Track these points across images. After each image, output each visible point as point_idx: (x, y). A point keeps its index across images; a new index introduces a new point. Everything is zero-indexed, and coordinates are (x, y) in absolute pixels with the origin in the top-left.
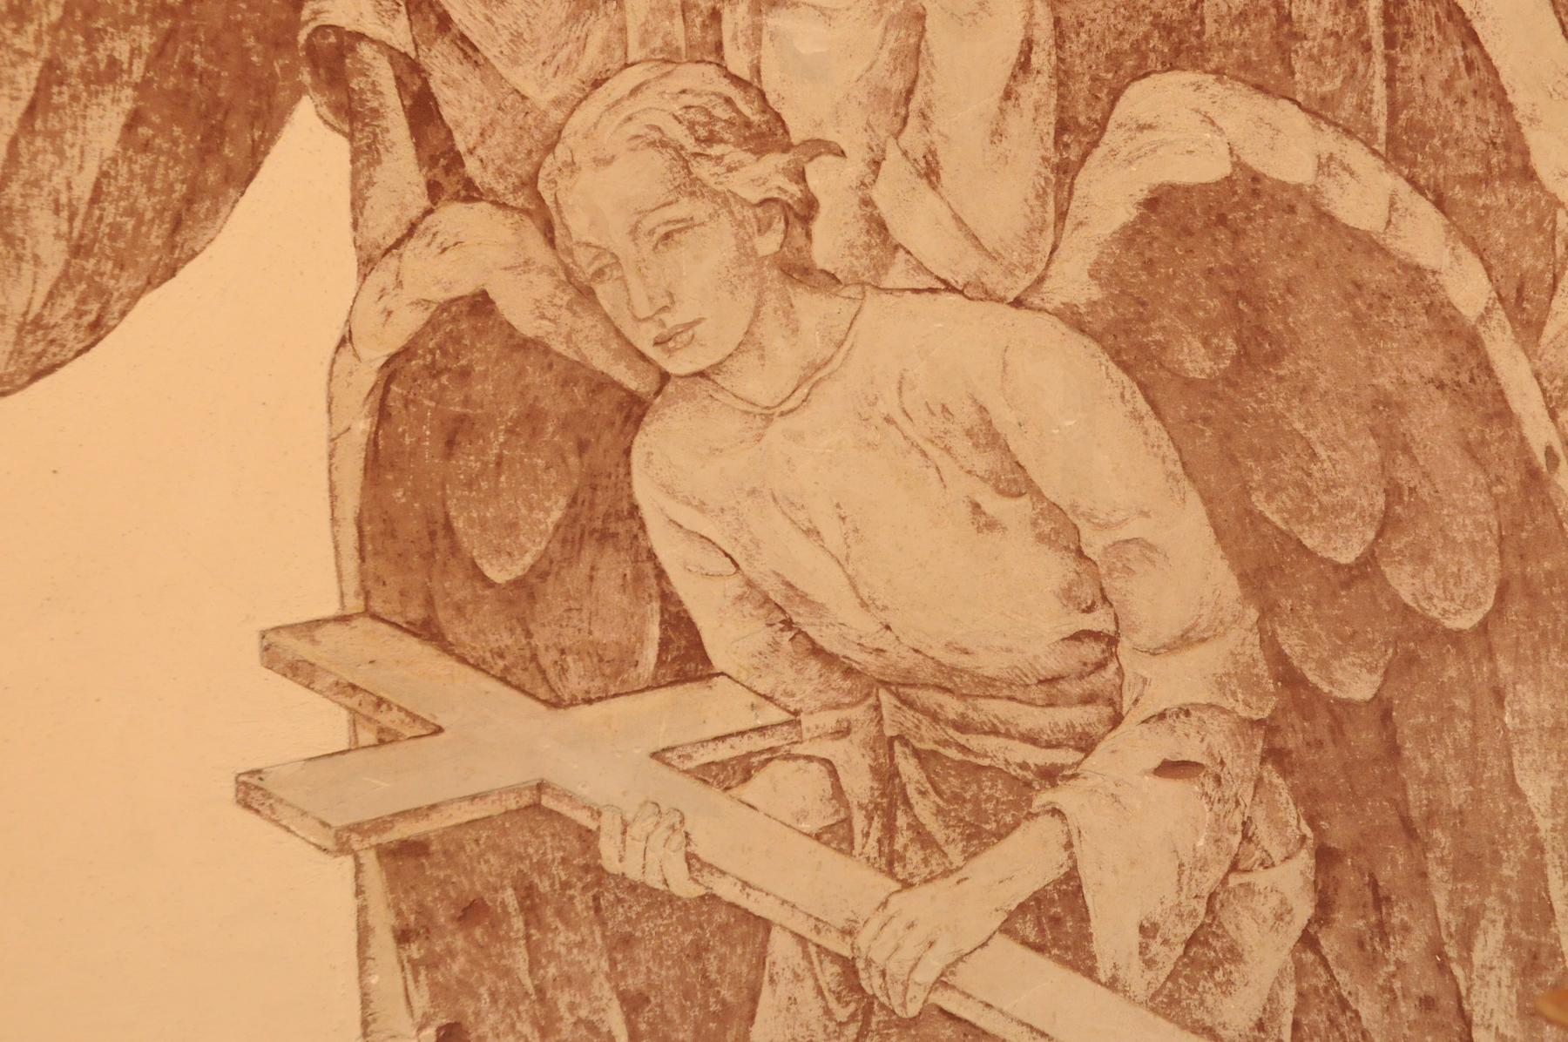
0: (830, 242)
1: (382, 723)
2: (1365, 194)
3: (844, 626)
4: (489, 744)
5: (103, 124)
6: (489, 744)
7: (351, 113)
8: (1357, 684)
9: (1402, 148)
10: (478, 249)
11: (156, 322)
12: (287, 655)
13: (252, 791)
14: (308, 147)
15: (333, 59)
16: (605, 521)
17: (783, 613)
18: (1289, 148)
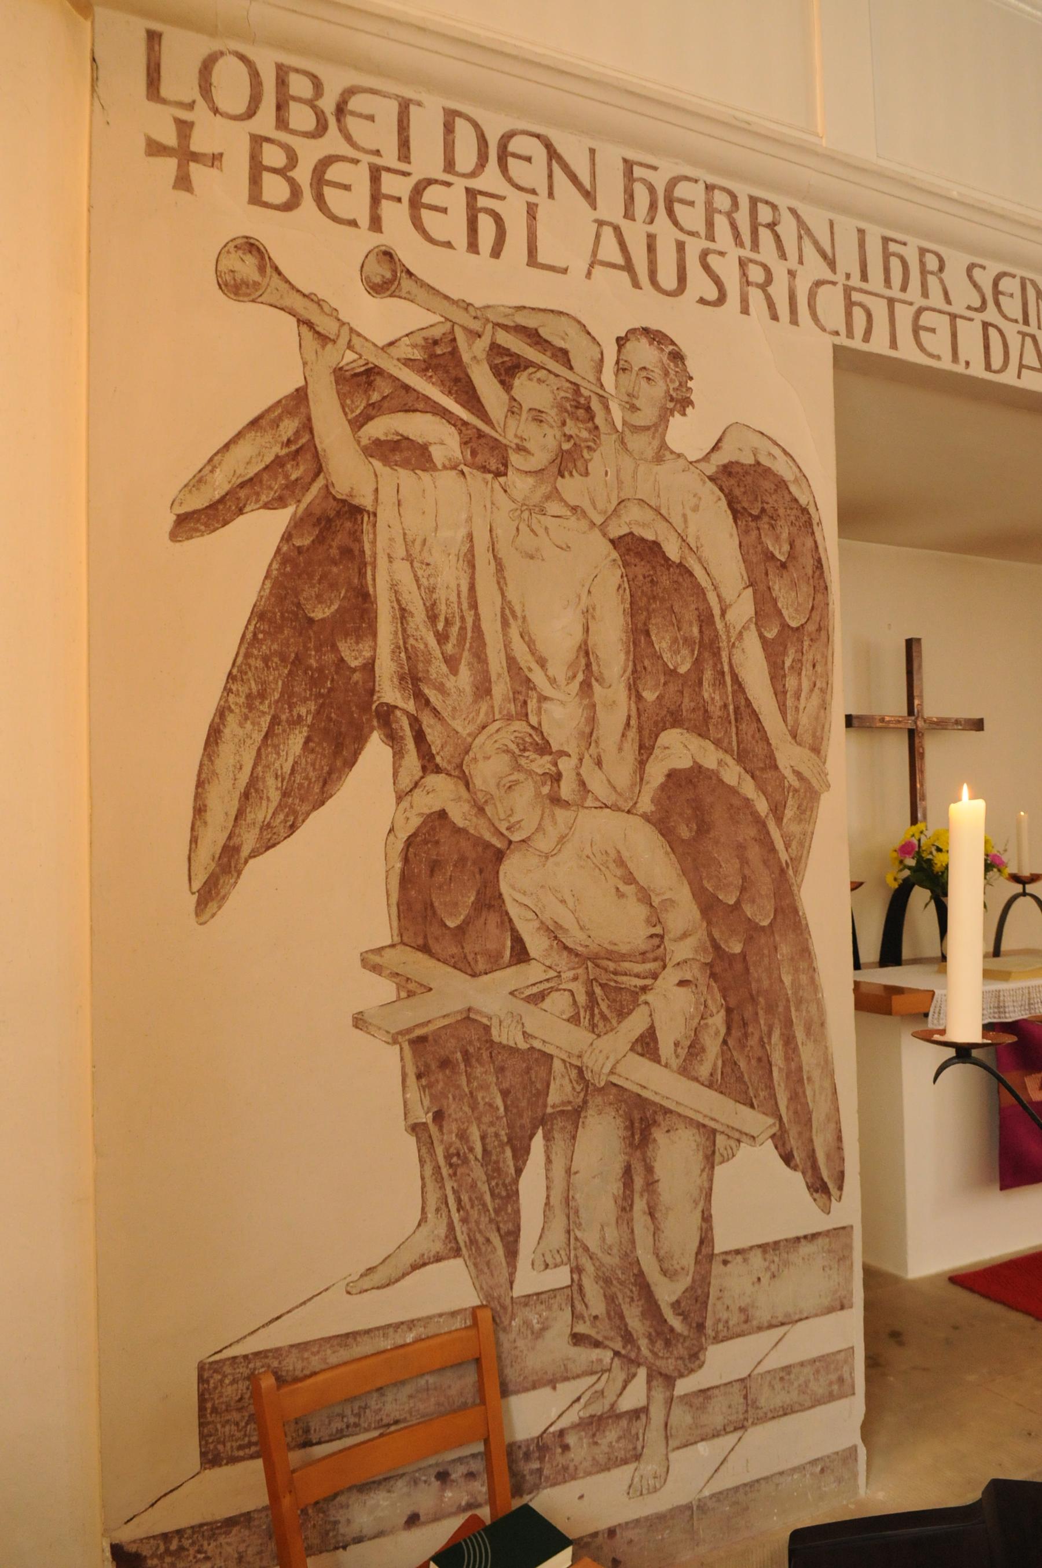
0: (567, 789)
1: (410, 989)
2: (732, 774)
3: (575, 938)
4: (452, 993)
5: (296, 742)
6: (452, 993)
7: (392, 738)
8: (737, 948)
9: (742, 757)
10: (441, 793)
11: (317, 824)
12: (371, 962)
13: (359, 1021)
14: (376, 752)
15: (386, 716)
16: (490, 901)
17: (553, 932)
18: (710, 757)
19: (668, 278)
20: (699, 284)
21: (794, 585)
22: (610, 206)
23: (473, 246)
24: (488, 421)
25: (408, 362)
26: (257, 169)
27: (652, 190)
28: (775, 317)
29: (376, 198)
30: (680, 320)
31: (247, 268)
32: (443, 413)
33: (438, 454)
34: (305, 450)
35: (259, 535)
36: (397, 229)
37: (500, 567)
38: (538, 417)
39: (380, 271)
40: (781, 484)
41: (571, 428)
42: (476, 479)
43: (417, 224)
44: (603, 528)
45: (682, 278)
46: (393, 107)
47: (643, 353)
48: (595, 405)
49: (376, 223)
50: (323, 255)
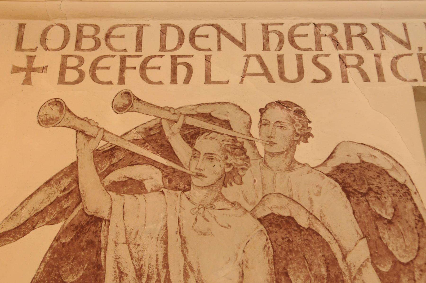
19: (291, 72)
20: (312, 72)
21: (401, 234)
22: (255, 45)
23: (174, 81)
24: (177, 161)
25: (134, 141)
26: (64, 68)
27: (280, 34)
28: (367, 80)
29: (122, 70)
30: (300, 94)
31: (54, 112)
32: (153, 163)
33: (148, 185)
34: (74, 193)
35: (45, 236)
36: (134, 82)
37: (184, 242)
38: (210, 157)
39: (122, 101)
40: (382, 172)
41: (231, 160)
42: (171, 195)
43: (144, 77)
44: (253, 213)
45: (301, 72)
46: (135, 30)
47: (277, 114)
48: (247, 145)
49: (122, 80)
50: (92, 101)
